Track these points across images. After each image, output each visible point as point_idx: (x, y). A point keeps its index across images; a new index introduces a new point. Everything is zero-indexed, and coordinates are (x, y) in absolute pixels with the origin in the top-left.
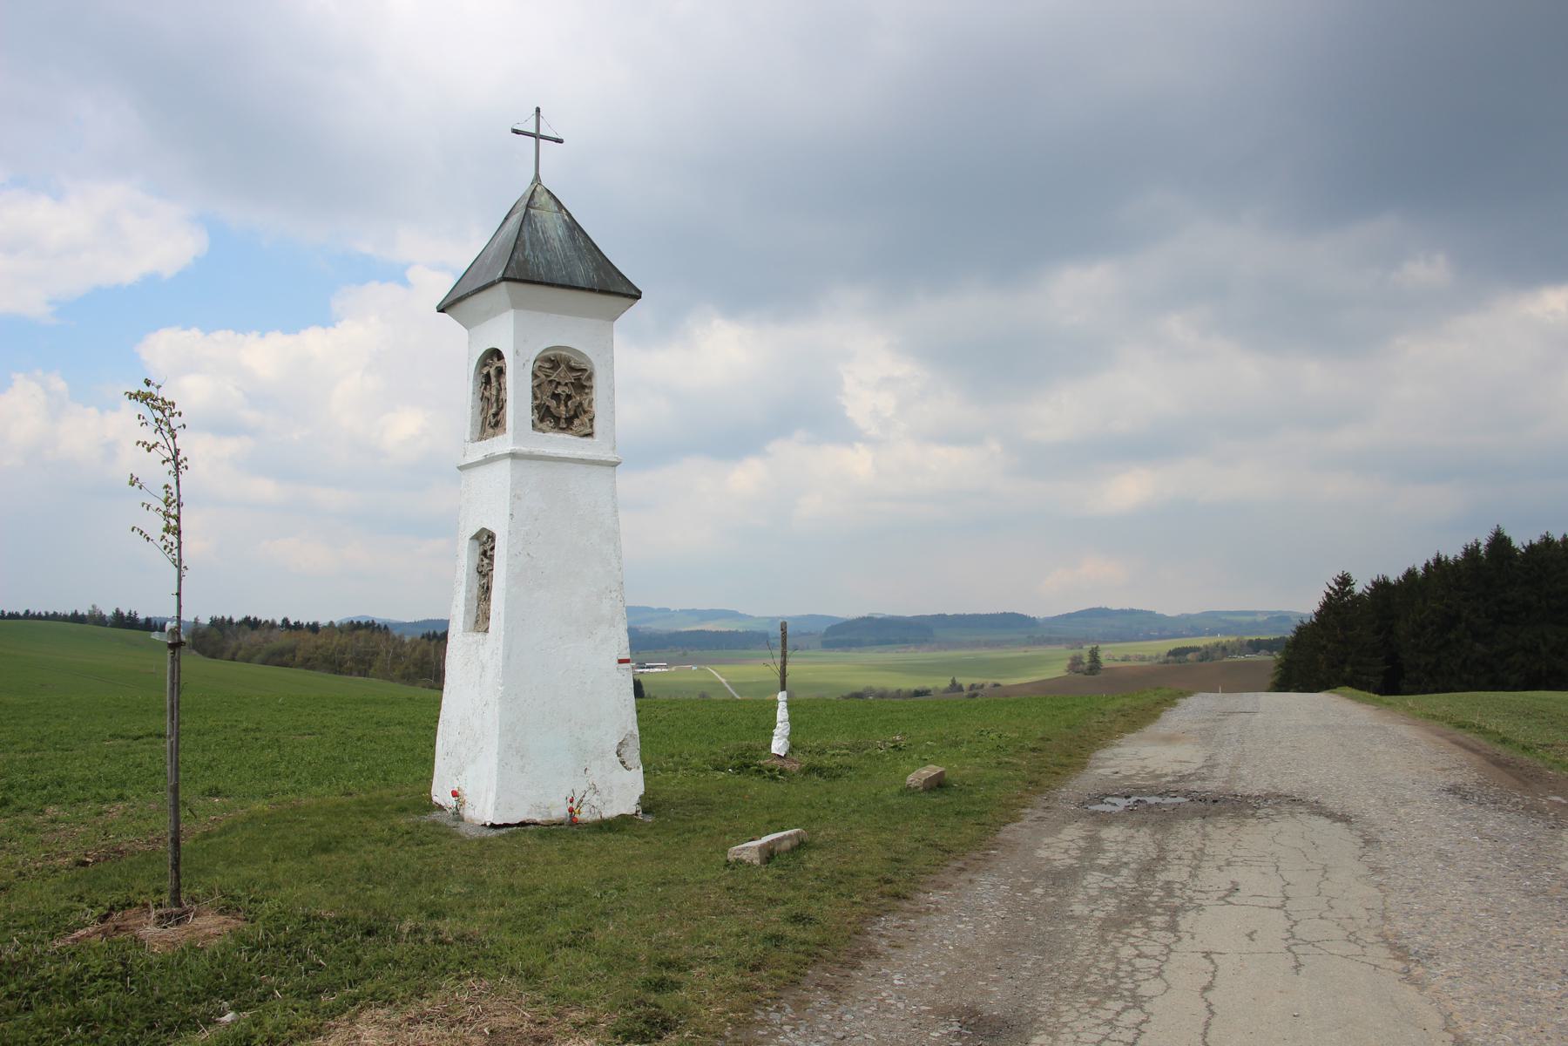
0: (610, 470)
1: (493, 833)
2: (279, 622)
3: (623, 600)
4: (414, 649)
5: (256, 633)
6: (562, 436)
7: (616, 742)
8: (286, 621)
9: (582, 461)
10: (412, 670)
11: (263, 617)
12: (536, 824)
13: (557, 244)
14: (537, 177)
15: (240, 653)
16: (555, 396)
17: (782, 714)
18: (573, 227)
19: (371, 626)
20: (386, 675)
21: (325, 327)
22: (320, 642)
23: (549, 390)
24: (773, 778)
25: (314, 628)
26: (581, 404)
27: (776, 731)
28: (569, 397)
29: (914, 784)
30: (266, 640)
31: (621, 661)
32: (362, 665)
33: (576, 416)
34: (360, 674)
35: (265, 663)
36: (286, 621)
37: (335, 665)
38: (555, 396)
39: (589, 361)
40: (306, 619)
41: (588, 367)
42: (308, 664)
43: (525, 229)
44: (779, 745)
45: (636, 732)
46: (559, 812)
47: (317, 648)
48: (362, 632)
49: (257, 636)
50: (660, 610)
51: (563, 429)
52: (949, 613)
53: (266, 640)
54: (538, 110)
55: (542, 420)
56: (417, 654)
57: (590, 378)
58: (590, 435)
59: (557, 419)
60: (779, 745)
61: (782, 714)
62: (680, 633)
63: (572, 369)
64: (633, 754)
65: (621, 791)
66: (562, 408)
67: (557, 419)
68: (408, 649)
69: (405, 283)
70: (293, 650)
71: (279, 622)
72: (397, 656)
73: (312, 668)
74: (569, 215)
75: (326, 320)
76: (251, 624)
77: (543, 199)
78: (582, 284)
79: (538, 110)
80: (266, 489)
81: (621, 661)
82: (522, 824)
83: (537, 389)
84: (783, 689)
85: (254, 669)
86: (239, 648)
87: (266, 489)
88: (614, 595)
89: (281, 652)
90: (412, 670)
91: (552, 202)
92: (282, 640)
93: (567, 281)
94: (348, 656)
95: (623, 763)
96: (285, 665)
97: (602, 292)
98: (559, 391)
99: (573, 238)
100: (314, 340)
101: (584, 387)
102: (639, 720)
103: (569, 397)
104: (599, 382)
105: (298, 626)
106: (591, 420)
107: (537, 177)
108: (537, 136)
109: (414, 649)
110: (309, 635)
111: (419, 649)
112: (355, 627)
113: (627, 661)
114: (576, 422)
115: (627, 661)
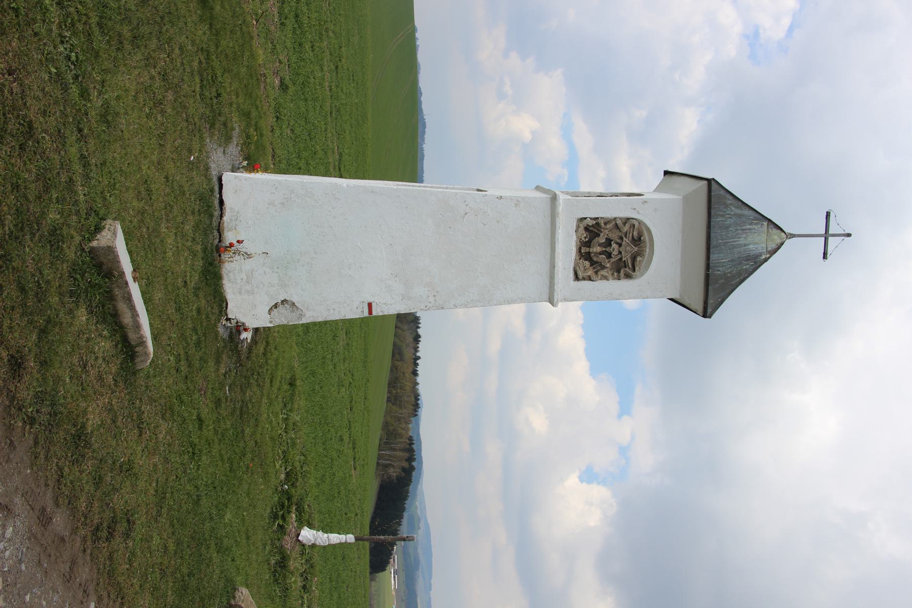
0: (546, 297)
1: (215, 179)
2: (418, 354)
3: (427, 309)
4: (403, 429)
5: (411, 340)
6: (574, 250)
7: (295, 299)
8: (419, 358)
9: (553, 266)
10: (391, 428)
11: (421, 345)
12: (221, 216)
13: (742, 241)
14: (793, 236)
15: (400, 331)
16: (609, 242)
17: (335, 538)
18: (756, 262)
19: (416, 406)
20: (388, 412)
21: (591, 375)
22: (407, 375)
23: (614, 236)
24: (275, 516)
25: (415, 373)
26: (603, 268)
27: (320, 533)
28: (609, 256)
29: (238, 594)
30: (407, 345)
31: (370, 305)
32: (394, 399)
33: (593, 264)
34: (388, 398)
35: (395, 344)
36: (419, 358)
37: (394, 383)
38: (609, 242)
39: (642, 275)
40: (420, 369)
41: (637, 273)
42: (394, 368)
43: (751, 212)
44: (307, 535)
45: (304, 321)
46: (230, 237)
47: (403, 373)
48: (413, 399)
49: (410, 339)
50: (430, 584)
51: (579, 250)
52: (433, 594)
53: (407, 345)
54: (849, 235)
55: (586, 229)
56: (400, 431)
57: (628, 276)
58: (577, 278)
59: (588, 244)
60: (307, 535)
61: (335, 538)
62: (416, 596)
63: (634, 259)
64: (283, 318)
65: (250, 300)
66: (599, 249)
67: (588, 244)
68: (403, 425)
69: (620, 416)
70: (402, 360)
71: (418, 354)
72: (399, 419)
73: (392, 371)
74: (766, 260)
75: (594, 371)
76: (417, 338)
77: (776, 237)
78: (713, 257)
79: (849, 235)
80: (495, 346)
81: (370, 305)
82: (221, 203)
83: (616, 225)
84: (357, 539)
85: (391, 338)
86: (403, 330)
87: (495, 346)
88: (431, 299)
89: (401, 354)
90: (391, 428)
91: (774, 246)
92: (408, 354)
93: (713, 243)
94: (399, 390)
95: (276, 306)
96: (393, 356)
97: (707, 277)
98: (614, 245)
99: (748, 259)
100: (581, 366)
101: (619, 271)
102: (314, 324)
103: (609, 256)
104: (624, 283)
105: (416, 365)
106: (590, 279)
107: (793, 236)
108: (826, 236)
109: (403, 429)
110: (411, 369)
111: (403, 432)
112: (417, 397)
113: (370, 312)
114: (587, 263)
115: (370, 312)
